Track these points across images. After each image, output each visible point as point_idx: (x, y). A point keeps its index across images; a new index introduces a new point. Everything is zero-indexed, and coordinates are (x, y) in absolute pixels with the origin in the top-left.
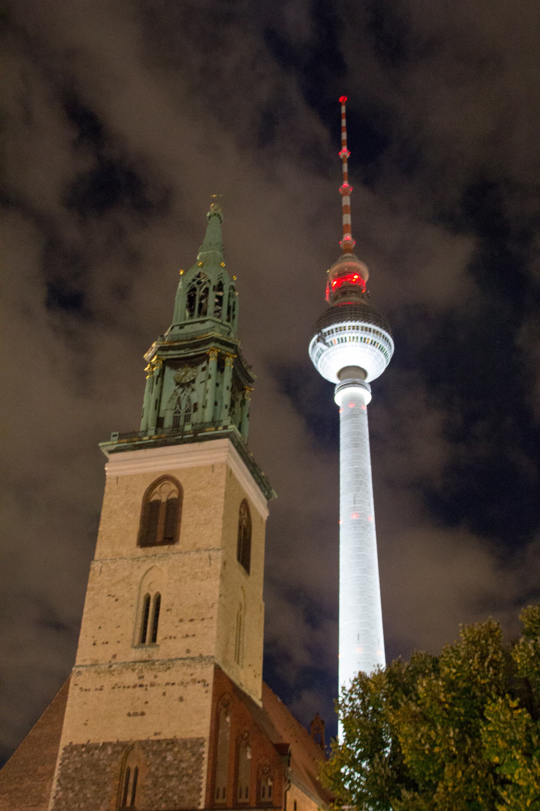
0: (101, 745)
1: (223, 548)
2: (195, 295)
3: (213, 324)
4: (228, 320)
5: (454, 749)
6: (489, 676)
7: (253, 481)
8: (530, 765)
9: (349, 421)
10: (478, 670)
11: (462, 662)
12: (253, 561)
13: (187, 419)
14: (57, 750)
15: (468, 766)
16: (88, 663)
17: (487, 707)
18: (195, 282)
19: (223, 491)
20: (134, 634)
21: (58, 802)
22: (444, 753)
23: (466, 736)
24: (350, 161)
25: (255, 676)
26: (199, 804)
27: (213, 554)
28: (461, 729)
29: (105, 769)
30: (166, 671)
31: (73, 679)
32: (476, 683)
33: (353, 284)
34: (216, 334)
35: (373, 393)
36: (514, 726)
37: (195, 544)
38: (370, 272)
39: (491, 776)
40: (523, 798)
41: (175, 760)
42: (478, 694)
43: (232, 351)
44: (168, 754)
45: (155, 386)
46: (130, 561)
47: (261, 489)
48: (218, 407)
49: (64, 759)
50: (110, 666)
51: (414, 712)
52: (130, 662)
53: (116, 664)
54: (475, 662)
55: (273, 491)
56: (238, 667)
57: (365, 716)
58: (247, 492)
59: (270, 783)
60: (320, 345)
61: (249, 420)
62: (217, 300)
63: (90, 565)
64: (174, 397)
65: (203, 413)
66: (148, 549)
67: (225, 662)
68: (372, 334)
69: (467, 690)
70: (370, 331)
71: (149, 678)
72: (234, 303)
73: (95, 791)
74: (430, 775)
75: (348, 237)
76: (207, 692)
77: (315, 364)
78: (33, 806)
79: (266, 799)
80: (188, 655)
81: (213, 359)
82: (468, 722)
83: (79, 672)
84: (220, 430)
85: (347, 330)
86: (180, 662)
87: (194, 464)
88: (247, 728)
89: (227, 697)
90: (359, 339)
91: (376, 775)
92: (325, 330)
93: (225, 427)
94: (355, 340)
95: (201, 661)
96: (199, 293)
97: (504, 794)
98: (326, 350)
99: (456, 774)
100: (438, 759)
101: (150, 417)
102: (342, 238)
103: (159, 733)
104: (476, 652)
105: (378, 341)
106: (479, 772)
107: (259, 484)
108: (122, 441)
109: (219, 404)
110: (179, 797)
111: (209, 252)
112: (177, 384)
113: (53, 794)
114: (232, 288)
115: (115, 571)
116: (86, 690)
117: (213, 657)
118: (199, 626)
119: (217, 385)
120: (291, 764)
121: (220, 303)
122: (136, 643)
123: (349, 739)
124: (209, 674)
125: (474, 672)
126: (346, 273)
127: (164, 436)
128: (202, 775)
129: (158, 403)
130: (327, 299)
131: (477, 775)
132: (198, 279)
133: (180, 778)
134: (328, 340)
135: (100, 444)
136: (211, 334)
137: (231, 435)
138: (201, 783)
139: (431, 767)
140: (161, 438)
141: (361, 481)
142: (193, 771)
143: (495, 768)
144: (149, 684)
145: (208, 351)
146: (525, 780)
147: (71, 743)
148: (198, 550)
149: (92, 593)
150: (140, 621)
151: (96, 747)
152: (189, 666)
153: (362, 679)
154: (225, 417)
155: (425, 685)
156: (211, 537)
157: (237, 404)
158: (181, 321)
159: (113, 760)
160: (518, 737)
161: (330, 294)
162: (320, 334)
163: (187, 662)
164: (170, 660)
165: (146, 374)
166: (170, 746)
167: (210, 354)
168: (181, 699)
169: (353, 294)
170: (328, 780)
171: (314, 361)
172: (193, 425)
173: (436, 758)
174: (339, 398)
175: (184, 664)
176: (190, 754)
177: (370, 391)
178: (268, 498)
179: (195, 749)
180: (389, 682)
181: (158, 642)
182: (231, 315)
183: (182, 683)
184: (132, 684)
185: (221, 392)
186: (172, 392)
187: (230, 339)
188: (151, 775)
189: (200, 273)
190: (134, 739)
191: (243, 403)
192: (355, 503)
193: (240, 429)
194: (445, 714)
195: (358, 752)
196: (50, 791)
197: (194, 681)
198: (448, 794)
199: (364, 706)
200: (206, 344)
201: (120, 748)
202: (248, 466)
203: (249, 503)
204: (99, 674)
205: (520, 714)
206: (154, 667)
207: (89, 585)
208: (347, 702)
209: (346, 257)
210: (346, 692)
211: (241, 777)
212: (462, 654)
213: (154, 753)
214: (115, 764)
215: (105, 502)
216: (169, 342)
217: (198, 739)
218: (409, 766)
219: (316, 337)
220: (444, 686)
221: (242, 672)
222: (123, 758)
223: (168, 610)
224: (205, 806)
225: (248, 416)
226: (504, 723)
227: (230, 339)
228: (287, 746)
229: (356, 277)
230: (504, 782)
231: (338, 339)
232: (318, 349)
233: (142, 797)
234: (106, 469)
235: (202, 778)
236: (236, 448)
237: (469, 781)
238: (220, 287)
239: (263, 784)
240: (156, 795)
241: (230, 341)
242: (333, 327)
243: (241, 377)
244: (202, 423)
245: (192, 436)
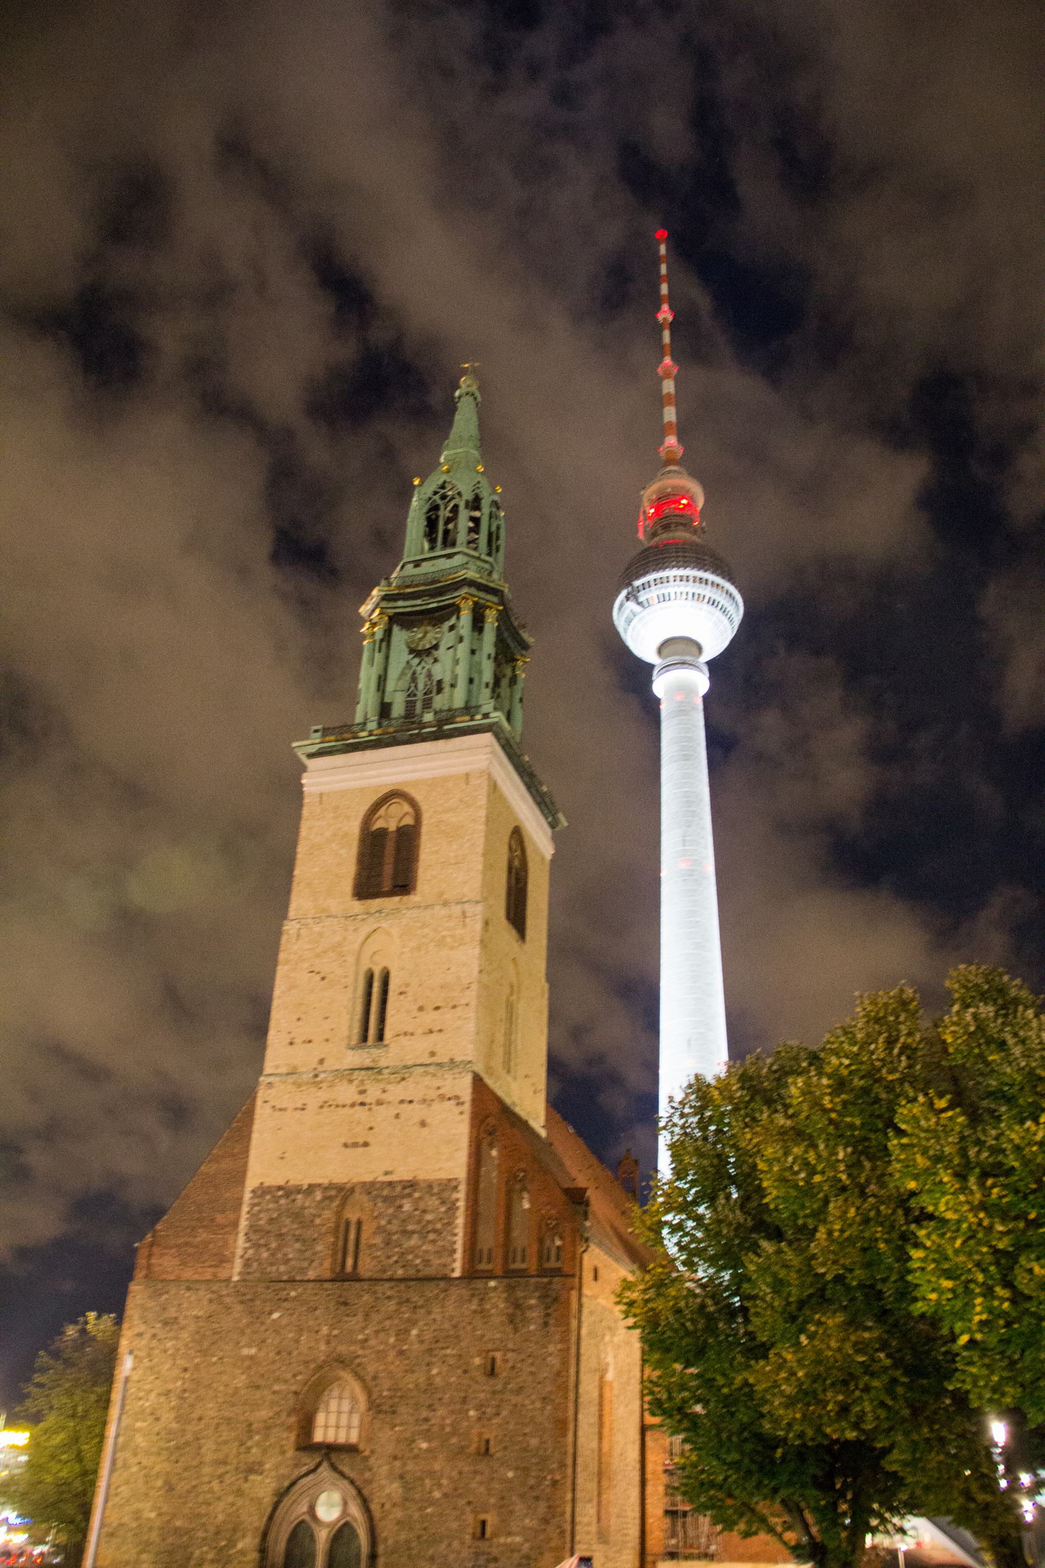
0: (305, 1187)
1: (485, 899)
2: (437, 517)
3: (466, 559)
4: (489, 554)
5: (844, 1177)
6: (900, 1069)
10: (883, 1060)
11: (860, 1048)
12: (530, 921)
13: (427, 704)
14: (242, 1191)
15: (865, 1200)
16: (283, 1070)
17: (900, 1110)
18: (437, 497)
19: (483, 813)
20: (350, 1027)
21: (247, 1264)
22: (829, 1183)
23: (863, 1158)
24: (674, 326)
25: (535, 1092)
26: (453, 1270)
27: (469, 909)
28: (855, 1147)
29: (312, 1221)
30: (399, 1082)
31: (261, 1094)
32: (880, 1080)
33: (681, 513)
34: (471, 574)
35: (712, 678)
36: (942, 1135)
37: (442, 894)
38: (706, 500)
39: (900, 1212)
41: (416, 1210)
42: (884, 1096)
43: (495, 599)
44: (405, 1201)
45: (377, 655)
46: (343, 920)
47: (542, 811)
48: (475, 687)
49: (253, 1205)
50: (316, 1076)
51: (782, 1127)
53: (324, 1072)
54: (879, 1048)
55: (561, 816)
56: (509, 1079)
57: (705, 1139)
58: (522, 817)
59: (558, 1243)
60: (631, 605)
61: (522, 707)
62: (471, 524)
63: (282, 925)
64: (407, 671)
65: (451, 696)
66: (369, 901)
67: (489, 1069)
68: (709, 586)
69: (865, 1091)
70: (706, 583)
71: (373, 1092)
72: (498, 528)
73: (300, 1251)
74: (806, 1216)
75: (671, 440)
78: (211, 1266)
79: (552, 1264)
82: (866, 1139)
83: (269, 1083)
85: (672, 582)
86: (422, 1069)
87: (438, 773)
88: (523, 1165)
89: (492, 1121)
90: (690, 595)
91: (720, 1222)
92: (637, 583)
93: (486, 716)
96: (444, 513)
97: (921, 1233)
99: (846, 1212)
100: (819, 1193)
101: (370, 702)
102: (662, 442)
104: (880, 1033)
105: (718, 599)
106: (882, 1208)
108: (327, 739)
109: (476, 681)
110: (423, 1261)
111: (459, 451)
112: (412, 651)
113: (239, 1252)
114: (495, 504)
115: (321, 935)
116: (280, 1110)
117: (470, 1062)
118: (448, 1016)
119: (473, 652)
120: (590, 1216)
121: (475, 530)
122: (354, 1042)
123: (679, 1173)
124: (464, 1087)
125: (878, 1064)
126: (669, 494)
127: (391, 730)
128: (456, 1231)
129: (382, 681)
130: (641, 536)
131: (878, 1212)
132: (443, 491)
133: (423, 1234)
134: (643, 596)
135: (294, 745)
136: (463, 574)
137: (494, 728)
138: (455, 1243)
139: (808, 1204)
140: (388, 733)
141: (694, 812)
142: (444, 1225)
143: (908, 1199)
144: (374, 1101)
145: (457, 601)
146: (956, 1211)
147: (262, 1184)
148: (446, 904)
149: (286, 967)
150: (359, 1009)
151: (298, 1190)
152: (434, 1075)
153: (699, 1088)
155: (800, 1085)
156: (465, 883)
157: (505, 682)
158: (416, 555)
159: (323, 1209)
160: (947, 1150)
161: (645, 528)
162: (630, 589)
163: (431, 1069)
164: (406, 1067)
165: (363, 637)
166: (407, 1191)
167: (462, 605)
168: (423, 1124)
169: (680, 527)
170: (648, 1233)
172: (436, 713)
173: (815, 1191)
174: (660, 686)
175: (426, 1073)
176: (437, 1202)
177: (708, 674)
178: (553, 825)
179: (446, 1195)
180: (742, 1088)
181: (386, 1042)
182: (494, 547)
183: (424, 1101)
184: (349, 1102)
185: (480, 664)
186: (403, 665)
187: (493, 582)
188: (380, 1230)
189: (445, 482)
190: (355, 1180)
191: (513, 680)
192: (684, 845)
193: (509, 717)
194: (831, 1129)
195: (693, 1191)
196: (235, 1248)
198: (833, 1241)
199: (703, 1125)
200: (456, 590)
201: (333, 1193)
202: (521, 777)
203: (524, 833)
204: (299, 1086)
205: (951, 1118)
206: (380, 1077)
207: (282, 956)
208: (676, 1119)
209: (669, 472)
210: (675, 1105)
211: (515, 1234)
212: (859, 1036)
213: (386, 1199)
214: (327, 1214)
215: (304, 832)
216: (398, 587)
217: (450, 1180)
218: (772, 1206)
219: (624, 593)
220: (829, 1086)
221: (514, 1086)
222: (338, 1206)
223: (401, 993)
225: (521, 700)
226: (927, 1131)
227: (493, 582)
228: (583, 1191)
229: (684, 501)
230: (924, 1217)
233: (368, 1260)
234: (304, 781)
235: (455, 1235)
236: (503, 747)
237: (866, 1221)
238: (475, 503)
239: (548, 1243)
240: (389, 1257)
241: (492, 585)
242: (650, 577)
243: (509, 640)
244: (450, 710)
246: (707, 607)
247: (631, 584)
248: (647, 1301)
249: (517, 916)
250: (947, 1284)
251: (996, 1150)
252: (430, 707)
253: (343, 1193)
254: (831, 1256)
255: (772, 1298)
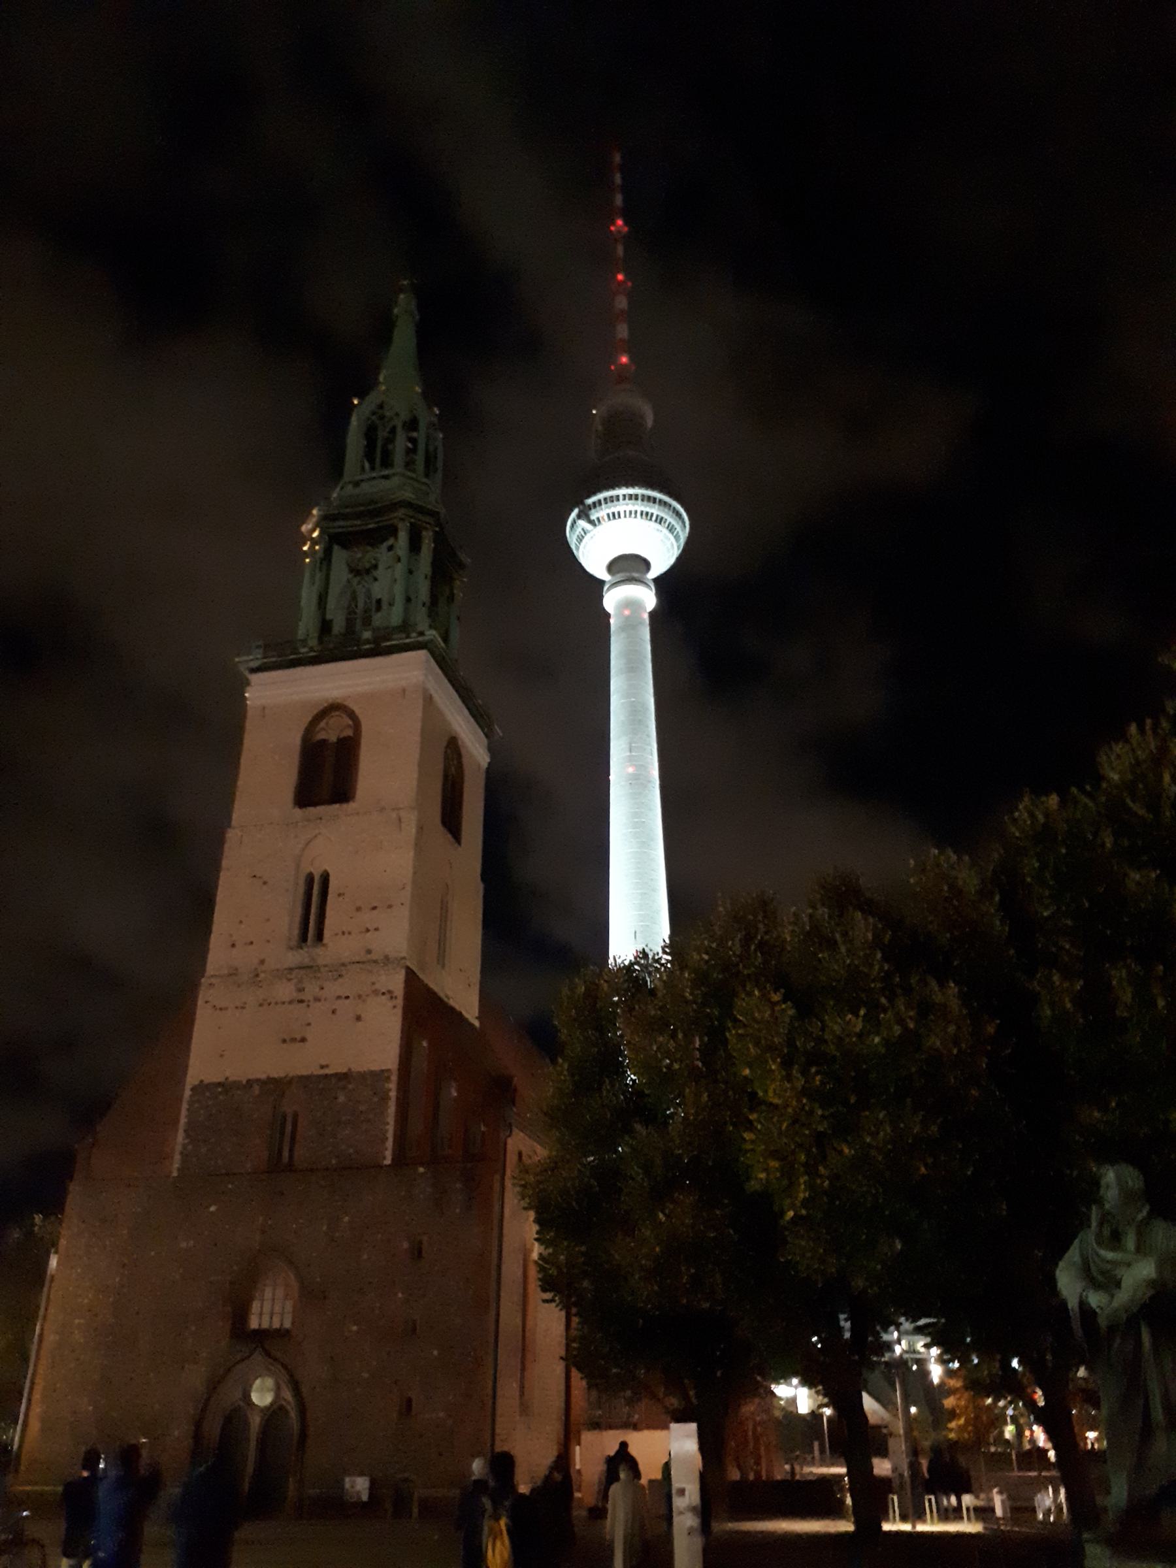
0: (244, 1082)
5: (700, 1064)
7: (466, 712)
8: (788, 1078)
9: (623, 635)
11: (718, 945)
13: (367, 622)
30: (336, 980)
34: (408, 495)
40: (778, 1121)
49: (191, 1103)
50: (257, 975)
52: (286, 969)
53: (264, 972)
54: (735, 946)
60: (582, 523)
62: (410, 445)
66: (311, 809)
71: (311, 989)
76: (395, 1007)
77: (575, 552)
80: (369, 956)
81: (403, 533)
84: (414, 637)
92: (590, 501)
94: (633, 515)
95: (385, 965)
96: (382, 434)
98: (592, 530)
103: (327, 1066)
105: (665, 516)
107: (474, 716)
113: (179, 1148)
116: (221, 1009)
117: (404, 958)
119: (411, 572)
121: (411, 452)
122: (294, 943)
124: (397, 982)
127: (331, 646)
132: (380, 411)
141: (640, 721)
145: (395, 521)
147: (202, 1081)
150: (299, 911)
151: (236, 1085)
152: (371, 972)
154: (421, 619)
164: (343, 965)
171: (573, 547)
174: (612, 600)
181: (325, 941)
183: (360, 996)
184: (287, 1000)
189: (383, 402)
190: (291, 1075)
191: (451, 598)
192: (631, 751)
193: (446, 639)
197: (376, 992)
207: (224, 863)
217: (382, 1071)
219: (576, 511)
223: (339, 895)
224: (393, 1160)
226: (757, 1022)
231: (608, 515)
232: (580, 529)
235: (388, 1124)
242: (601, 496)
245: (372, 646)
246: (653, 525)
247: (582, 503)
248: (540, 1182)
249: (451, 820)
250: (774, 1164)
251: (821, 1040)
252: (370, 625)
253: (275, 1087)
254: (688, 1139)
255: (643, 1179)
